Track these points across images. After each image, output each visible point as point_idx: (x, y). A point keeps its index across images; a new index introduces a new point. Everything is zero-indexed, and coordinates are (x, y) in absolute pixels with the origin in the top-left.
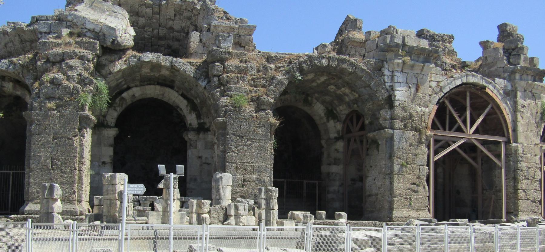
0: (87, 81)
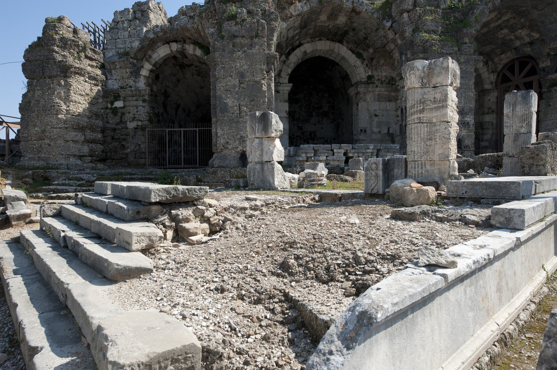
0: (273, 16)
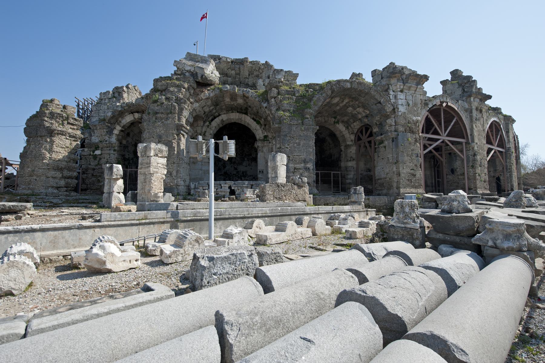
0: (182, 101)
